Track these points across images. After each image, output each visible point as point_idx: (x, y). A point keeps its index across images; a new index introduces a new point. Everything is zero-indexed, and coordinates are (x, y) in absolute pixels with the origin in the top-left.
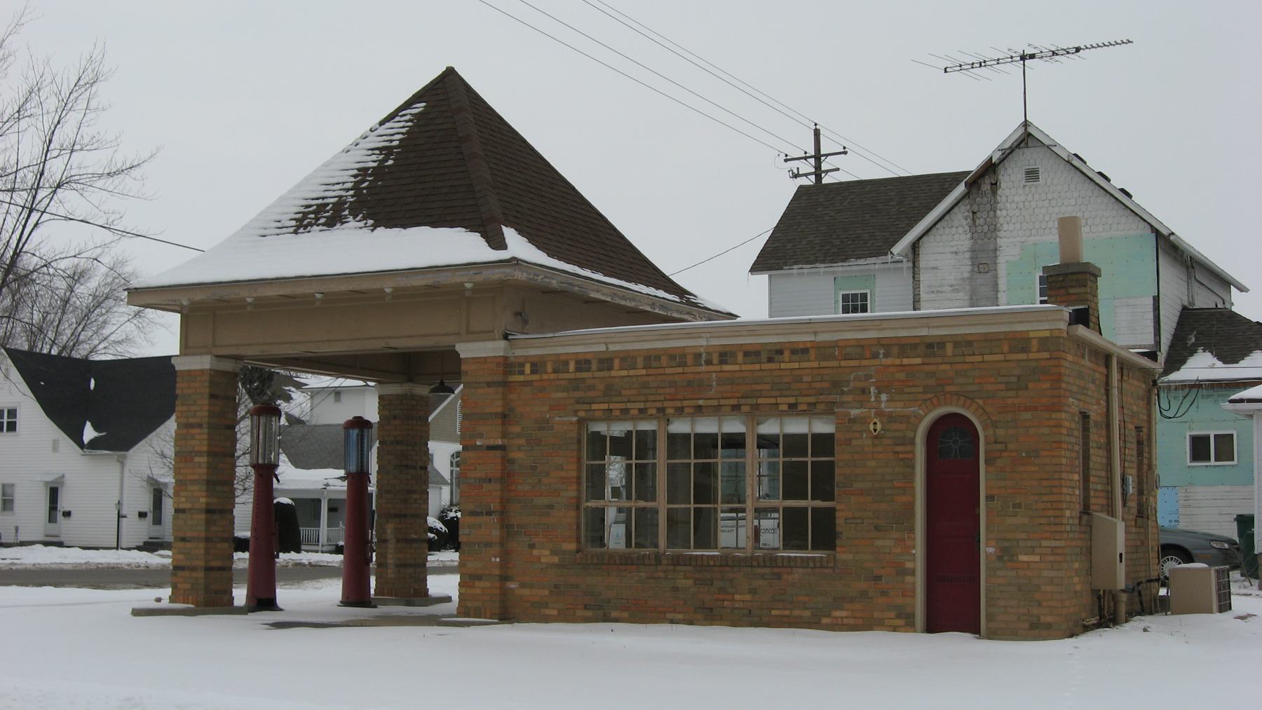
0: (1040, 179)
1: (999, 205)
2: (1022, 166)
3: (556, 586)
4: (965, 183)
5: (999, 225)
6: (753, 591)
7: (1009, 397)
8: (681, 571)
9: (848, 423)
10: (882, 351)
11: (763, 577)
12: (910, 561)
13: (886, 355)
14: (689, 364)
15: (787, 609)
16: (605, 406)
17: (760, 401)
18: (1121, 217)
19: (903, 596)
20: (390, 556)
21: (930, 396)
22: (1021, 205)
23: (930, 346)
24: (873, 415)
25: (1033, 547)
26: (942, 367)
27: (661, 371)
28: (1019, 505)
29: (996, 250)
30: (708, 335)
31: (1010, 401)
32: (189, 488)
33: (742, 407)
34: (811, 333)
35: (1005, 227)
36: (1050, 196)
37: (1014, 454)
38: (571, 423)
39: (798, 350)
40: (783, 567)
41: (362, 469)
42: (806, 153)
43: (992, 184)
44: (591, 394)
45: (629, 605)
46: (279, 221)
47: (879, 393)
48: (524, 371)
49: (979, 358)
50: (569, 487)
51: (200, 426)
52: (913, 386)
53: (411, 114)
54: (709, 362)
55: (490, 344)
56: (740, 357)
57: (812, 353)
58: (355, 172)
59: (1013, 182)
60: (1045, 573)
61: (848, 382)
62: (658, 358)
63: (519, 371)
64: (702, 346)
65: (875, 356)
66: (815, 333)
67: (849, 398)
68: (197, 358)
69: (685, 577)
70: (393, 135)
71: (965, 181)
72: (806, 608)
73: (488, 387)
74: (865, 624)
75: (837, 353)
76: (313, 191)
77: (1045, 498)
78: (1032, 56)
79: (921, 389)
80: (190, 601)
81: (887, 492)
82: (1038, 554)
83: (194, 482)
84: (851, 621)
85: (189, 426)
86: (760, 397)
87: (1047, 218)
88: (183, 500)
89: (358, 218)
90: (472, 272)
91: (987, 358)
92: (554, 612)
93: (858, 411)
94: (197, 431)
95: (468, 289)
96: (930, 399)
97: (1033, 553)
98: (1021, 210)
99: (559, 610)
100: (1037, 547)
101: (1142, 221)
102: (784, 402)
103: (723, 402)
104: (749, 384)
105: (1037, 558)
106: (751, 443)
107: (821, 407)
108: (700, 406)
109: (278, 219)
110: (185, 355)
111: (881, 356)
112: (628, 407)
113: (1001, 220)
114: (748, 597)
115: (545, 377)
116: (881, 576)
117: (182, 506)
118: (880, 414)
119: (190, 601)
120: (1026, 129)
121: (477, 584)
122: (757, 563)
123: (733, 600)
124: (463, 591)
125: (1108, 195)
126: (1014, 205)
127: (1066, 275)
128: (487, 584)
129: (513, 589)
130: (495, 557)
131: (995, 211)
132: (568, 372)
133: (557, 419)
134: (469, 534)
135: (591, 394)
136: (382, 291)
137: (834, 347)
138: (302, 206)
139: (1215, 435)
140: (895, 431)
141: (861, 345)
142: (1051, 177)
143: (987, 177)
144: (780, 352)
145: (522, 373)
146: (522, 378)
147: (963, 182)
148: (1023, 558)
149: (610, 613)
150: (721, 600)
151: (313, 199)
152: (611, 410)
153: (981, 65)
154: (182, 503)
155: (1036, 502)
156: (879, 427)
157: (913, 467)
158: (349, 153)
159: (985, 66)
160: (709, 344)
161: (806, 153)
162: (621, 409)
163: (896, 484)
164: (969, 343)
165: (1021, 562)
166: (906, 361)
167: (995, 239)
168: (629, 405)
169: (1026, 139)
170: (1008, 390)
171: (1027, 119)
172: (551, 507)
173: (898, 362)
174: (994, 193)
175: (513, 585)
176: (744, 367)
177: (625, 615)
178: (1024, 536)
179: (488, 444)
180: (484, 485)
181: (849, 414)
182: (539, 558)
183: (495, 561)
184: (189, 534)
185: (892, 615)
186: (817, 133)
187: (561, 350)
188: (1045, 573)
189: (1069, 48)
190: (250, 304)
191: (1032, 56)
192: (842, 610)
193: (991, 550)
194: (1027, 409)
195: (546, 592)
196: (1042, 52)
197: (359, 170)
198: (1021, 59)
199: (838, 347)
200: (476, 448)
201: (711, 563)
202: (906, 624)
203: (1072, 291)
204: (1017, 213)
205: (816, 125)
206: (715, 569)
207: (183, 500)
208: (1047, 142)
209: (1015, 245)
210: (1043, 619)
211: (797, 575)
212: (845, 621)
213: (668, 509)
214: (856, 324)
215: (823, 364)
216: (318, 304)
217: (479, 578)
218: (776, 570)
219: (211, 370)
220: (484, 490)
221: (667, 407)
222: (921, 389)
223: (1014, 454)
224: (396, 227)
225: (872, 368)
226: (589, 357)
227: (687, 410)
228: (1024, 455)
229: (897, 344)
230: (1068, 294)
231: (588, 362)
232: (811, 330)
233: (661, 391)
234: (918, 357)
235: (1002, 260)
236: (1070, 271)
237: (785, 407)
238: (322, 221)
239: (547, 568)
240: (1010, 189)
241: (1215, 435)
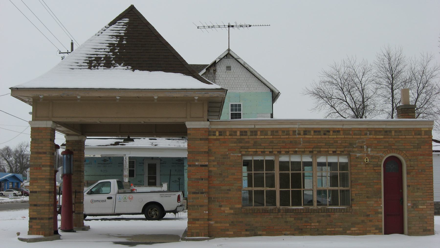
0: (232, 70)
1: (216, 78)
3: (232, 222)
4: (206, 69)
6: (319, 222)
7: (415, 151)
8: (288, 215)
9: (356, 159)
10: (368, 133)
11: (323, 216)
12: (380, 209)
13: (370, 134)
14: (269, 135)
15: (333, 228)
16: (254, 150)
17: (322, 150)
18: (260, 85)
19: (378, 221)
21: (386, 150)
22: (224, 79)
23: (386, 132)
24: (365, 156)
25: (424, 203)
26: (390, 139)
27: (279, 137)
28: (419, 189)
30: (300, 124)
31: (415, 152)
32: (39, 181)
33: (314, 152)
34: (342, 125)
36: (235, 76)
37: (417, 171)
38: (238, 156)
39: (336, 131)
40: (331, 212)
41: (71, 172)
42: (68, 51)
43: (214, 70)
44: (247, 145)
45: (266, 229)
46: (78, 63)
47: (368, 148)
48: (216, 134)
49: (404, 137)
50: (238, 182)
51: (45, 153)
52: (381, 146)
53: (123, 23)
54: (299, 134)
55: (203, 123)
56: (312, 133)
57: (341, 132)
58: (108, 45)
59: (222, 70)
60: (428, 212)
61: (356, 143)
62: (277, 132)
63: (213, 134)
64: (296, 128)
65: (366, 134)
66: (343, 125)
67: (356, 149)
68: (45, 122)
69: (290, 217)
70: (119, 30)
71: (206, 68)
72: (340, 227)
73: (200, 140)
74: (364, 232)
75: (351, 133)
76: (89, 51)
77: (428, 186)
78: (233, 26)
79: (383, 147)
81: (371, 184)
82: (425, 206)
83: (42, 179)
84: (358, 232)
86: (321, 148)
87: (234, 84)
89: (122, 65)
90: (203, 93)
91: (407, 137)
92: (232, 233)
93: (360, 154)
95: (196, 100)
96: (387, 150)
97: (424, 205)
98: (224, 80)
99: (234, 232)
100: (425, 203)
101: (267, 87)
102: (331, 150)
103: (306, 150)
104: (316, 143)
105: (425, 207)
106: (315, 165)
107: (345, 153)
108: (296, 151)
109: (77, 61)
110: (36, 120)
111: (368, 135)
112: (265, 150)
114: (317, 224)
115: (226, 137)
116: (370, 215)
117: (34, 190)
118: (368, 155)
120: (229, 52)
121: (197, 222)
122: (321, 211)
123: (311, 225)
124: (190, 225)
125: (256, 77)
126: (222, 78)
127: (408, 108)
128: (202, 222)
129: (212, 224)
130: (206, 211)
131: (215, 80)
132: (236, 136)
133: (232, 154)
134: (193, 202)
135: (247, 145)
136: (153, 97)
137: (350, 130)
138: (87, 57)
140: (373, 162)
141: (360, 130)
142: (235, 69)
143: (212, 67)
144: (329, 131)
145: (215, 135)
146: (215, 137)
147: (205, 68)
148: (421, 207)
149: (257, 232)
150: (306, 226)
151: (91, 55)
152: (257, 151)
155: (424, 187)
156: (368, 160)
157: (381, 175)
158: (99, 36)
159: (214, 28)
160: (299, 127)
161: (68, 51)
162: (261, 151)
163: (375, 181)
164: (400, 131)
165: (420, 208)
166: (378, 137)
168: (265, 150)
169: (228, 55)
170: (414, 148)
171: (230, 48)
172: (229, 190)
173: (374, 137)
174: (215, 73)
175: (212, 222)
176: (314, 137)
177: (264, 233)
178: (420, 199)
179: (202, 164)
180: (200, 181)
181: (356, 155)
182: (224, 211)
183: (206, 213)
184: (39, 203)
185: (374, 229)
186: (72, 44)
187: (233, 127)
188: (428, 212)
189: (243, 25)
190: (79, 99)
191: (233, 26)
192: (355, 227)
193: (409, 204)
194: (421, 155)
195: (228, 225)
196: (236, 25)
197: (109, 44)
198: (228, 27)
199: (352, 131)
200: (195, 165)
201: (302, 211)
202: (379, 232)
203: (410, 114)
204: (223, 81)
205: (72, 41)
206: (303, 214)
207: (36, 187)
208: (236, 57)
210: (428, 228)
211: (337, 215)
212: (356, 232)
213: (280, 191)
214: (359, 122)
215: (346, 137)
216: (118, 101)
217: (198, 220)
218: (329, 213)
219: (51, 128)
220: (200, 183)
221: (290, 151)
222: (383, 147)
223: (417, 171)
224: (145, 70)
225: (365, 139)
226: (246, 130)
227: (290, 152)
228: (420, 171)
229: (374, 131)
230: (409, 115)
231: (246, 132)
232: (342, 124)
233: (279, 144)
234: (382, 135)
236: (410, 107)
237: (331, 152)
238: (102, 65)
239: (228, 215)
240: (221, 72)
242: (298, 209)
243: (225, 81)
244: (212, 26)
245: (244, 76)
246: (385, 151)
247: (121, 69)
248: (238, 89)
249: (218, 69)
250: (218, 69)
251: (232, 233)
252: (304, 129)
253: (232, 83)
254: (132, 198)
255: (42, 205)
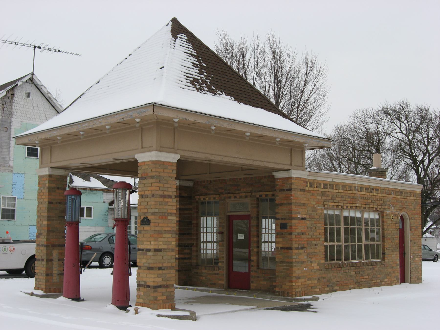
2: (24, 90)
5: (13, 112)
20: (54, 269)
22: (22, 106)
29: (11, 122)
30: (359, 180)
32: (165, 235)
35: (15, 114)
43: (11, 94)
47: (392, 206)
51: (170, 197)
59: (20, 96)
64: (356, 184)
68: (148, 154)
78: (39, 48)
80: (167, 306)
83: (167, 232)
85: (146, 196)
88: (161, 243)
90: (318, 141)
92: (318, 290)
94: (170, 200)
108: (357, 206)
113: (14, 110)
114: (367, 277)
117: (160, 247)
119: (167, 306)
125: (55, 110)
126: (20, 106)
130: (305, 268)
131: (12, 106)
133: (318, 207)
139: (86, 208)
153: (55, 51)
154: (160, 245)
167: (11, 118)
169: (31, 81)
174: (12, 99)
181: (386, 212)
184: (165, 265)
185: (395, 279)
191: (39, 48)
195: (316, 282)
204: (21, 109)
207: (161, 243)
209: (19, 122)
224: (250, 105)
226: (320, 182)
231: (326, 185)
233: (346, 199)
235: (13, 127)
241: (86, 208)
242: (375, 262)
243: (23, 109)
244: (15, 43)
245: (43, 107)
246: (400, 210)
247: (228, 99)
248: (37, 120)
249: (17, 94)
250: (17, 94)
251: (318, 290)
252: (360, 186)
253: (30, 113)
254: (14, 250)
255: (167, 268)
